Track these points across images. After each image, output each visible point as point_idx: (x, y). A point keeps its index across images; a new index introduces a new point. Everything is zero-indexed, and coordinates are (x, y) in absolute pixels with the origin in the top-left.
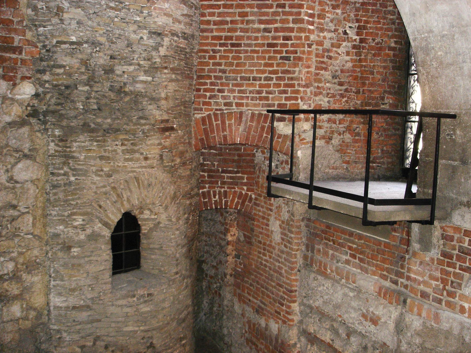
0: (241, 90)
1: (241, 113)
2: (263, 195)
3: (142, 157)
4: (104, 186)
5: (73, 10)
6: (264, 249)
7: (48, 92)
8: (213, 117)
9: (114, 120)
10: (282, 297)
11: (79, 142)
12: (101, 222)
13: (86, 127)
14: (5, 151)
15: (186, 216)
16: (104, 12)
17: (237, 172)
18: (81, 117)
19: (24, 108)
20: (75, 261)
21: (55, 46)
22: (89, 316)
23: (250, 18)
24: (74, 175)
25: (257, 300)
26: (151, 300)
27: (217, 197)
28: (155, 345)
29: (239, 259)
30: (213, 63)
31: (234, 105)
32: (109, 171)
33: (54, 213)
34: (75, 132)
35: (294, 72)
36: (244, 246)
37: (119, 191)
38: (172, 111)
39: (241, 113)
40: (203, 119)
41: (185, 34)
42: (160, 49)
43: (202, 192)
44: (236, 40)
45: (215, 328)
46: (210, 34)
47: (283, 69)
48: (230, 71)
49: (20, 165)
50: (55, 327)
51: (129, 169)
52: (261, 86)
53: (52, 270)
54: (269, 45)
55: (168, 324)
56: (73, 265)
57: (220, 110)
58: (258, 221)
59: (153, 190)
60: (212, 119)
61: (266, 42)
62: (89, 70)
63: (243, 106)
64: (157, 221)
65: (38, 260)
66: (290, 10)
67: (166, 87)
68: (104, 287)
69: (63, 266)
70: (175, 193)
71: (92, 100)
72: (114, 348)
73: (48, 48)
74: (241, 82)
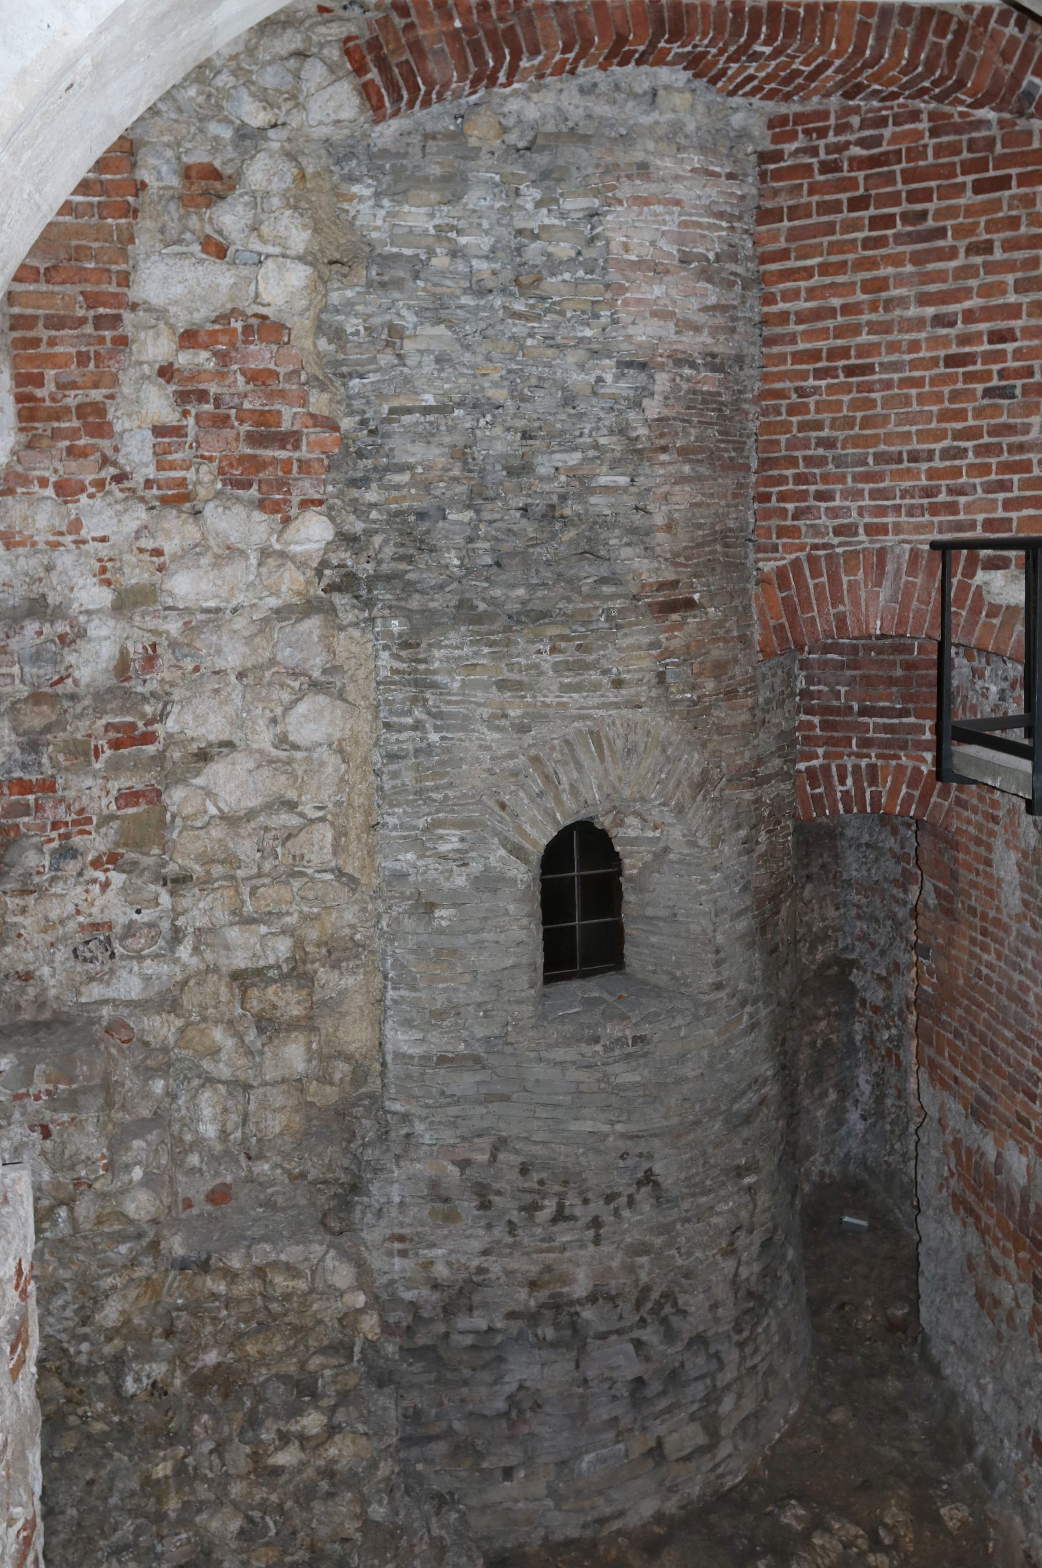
0: (878, 490)
1: (882, 553)
3: (605, 680)
4: (512, 756)
5: (429, 330)
6: (984, 932)
7: (376, 532)
8: (806, 566)
9: (532, 588)
11: (446, 647)
12: (504, 847)
13: (465, 612)
14: (268, 674)
15: (743, 833)
16: (499, 327)
17: (904, 713)
18: (454, 585)
19: (310, 573)
20: (445, 941)
21: (388, 421)
22: (479, 1083)
23: (895, 292)
24: (437, 729)
25: (974, 1079)
26: (645, 1055)
27: (849, 781)
28: (660, 1179)
29: (927, 957)
30: (799, 423)
31: (861, 531)
32: (523, 716)
33: (392, 821)
34: (438, 624)
35: (1027, 429)
36: (938, 922)
37: (550, 767)
38: (687, 559)
39: (882, 553)
40: (781, 572)
41: (714, 356)
42: (646, 402)
44: (858, 357)
45: (891, 1159)
46: (789, 349)
47: (993, 422)
48: (845, 441)
49: (302, 708)
50: (397, 1107)
51: (574, 712)
52: (932, 474)
53: (390, 961)
54: (952, 361)
55: (697, 1123)
56: (439, 951)
57: (825, 546)
58: (968, 851)
59: (639, 764)
61: (942, 353)
62: (470, 471)
63: (886, 533)
64: (661, 844)
65: (358, 937)
66: (1006, 256)
67: (666, 497)
68: (516, 1010)
69: (413, 952)
70: (705, 772)
71: (479, 544)
72: (544, 1175)
73: (372, 425)
74: (877, 468)
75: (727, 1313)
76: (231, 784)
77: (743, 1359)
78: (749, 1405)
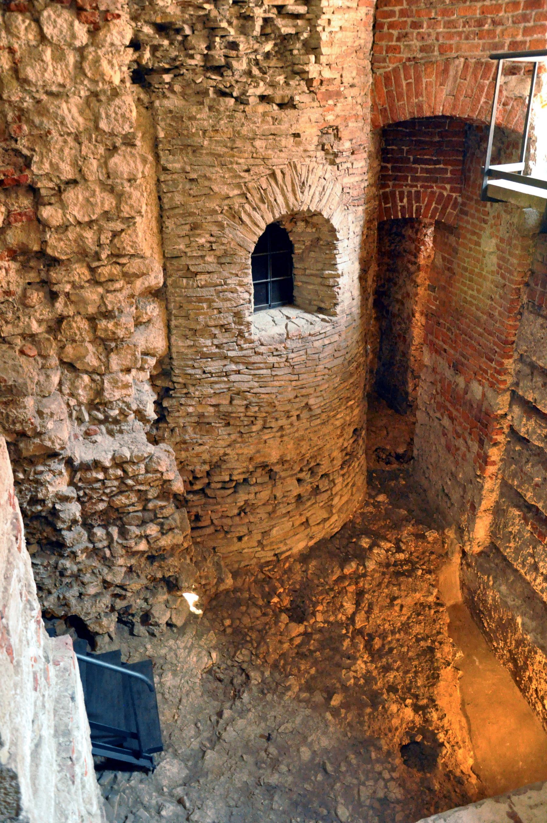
2: (475, 197)
8: (402, 71)
10: (492, 349)
27: (405, 200)
29: (434, 292)
43: (384, 193)
50: (180, 380)
60: (399, 77)
75: (338, 463)
76: (75, 205)
77: (344, 481)
78: (345, 499)
